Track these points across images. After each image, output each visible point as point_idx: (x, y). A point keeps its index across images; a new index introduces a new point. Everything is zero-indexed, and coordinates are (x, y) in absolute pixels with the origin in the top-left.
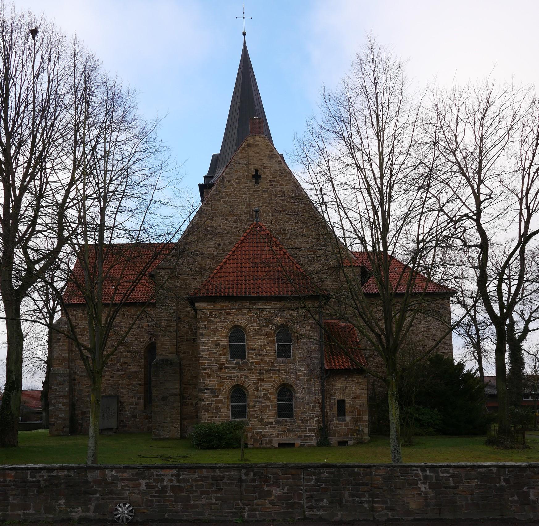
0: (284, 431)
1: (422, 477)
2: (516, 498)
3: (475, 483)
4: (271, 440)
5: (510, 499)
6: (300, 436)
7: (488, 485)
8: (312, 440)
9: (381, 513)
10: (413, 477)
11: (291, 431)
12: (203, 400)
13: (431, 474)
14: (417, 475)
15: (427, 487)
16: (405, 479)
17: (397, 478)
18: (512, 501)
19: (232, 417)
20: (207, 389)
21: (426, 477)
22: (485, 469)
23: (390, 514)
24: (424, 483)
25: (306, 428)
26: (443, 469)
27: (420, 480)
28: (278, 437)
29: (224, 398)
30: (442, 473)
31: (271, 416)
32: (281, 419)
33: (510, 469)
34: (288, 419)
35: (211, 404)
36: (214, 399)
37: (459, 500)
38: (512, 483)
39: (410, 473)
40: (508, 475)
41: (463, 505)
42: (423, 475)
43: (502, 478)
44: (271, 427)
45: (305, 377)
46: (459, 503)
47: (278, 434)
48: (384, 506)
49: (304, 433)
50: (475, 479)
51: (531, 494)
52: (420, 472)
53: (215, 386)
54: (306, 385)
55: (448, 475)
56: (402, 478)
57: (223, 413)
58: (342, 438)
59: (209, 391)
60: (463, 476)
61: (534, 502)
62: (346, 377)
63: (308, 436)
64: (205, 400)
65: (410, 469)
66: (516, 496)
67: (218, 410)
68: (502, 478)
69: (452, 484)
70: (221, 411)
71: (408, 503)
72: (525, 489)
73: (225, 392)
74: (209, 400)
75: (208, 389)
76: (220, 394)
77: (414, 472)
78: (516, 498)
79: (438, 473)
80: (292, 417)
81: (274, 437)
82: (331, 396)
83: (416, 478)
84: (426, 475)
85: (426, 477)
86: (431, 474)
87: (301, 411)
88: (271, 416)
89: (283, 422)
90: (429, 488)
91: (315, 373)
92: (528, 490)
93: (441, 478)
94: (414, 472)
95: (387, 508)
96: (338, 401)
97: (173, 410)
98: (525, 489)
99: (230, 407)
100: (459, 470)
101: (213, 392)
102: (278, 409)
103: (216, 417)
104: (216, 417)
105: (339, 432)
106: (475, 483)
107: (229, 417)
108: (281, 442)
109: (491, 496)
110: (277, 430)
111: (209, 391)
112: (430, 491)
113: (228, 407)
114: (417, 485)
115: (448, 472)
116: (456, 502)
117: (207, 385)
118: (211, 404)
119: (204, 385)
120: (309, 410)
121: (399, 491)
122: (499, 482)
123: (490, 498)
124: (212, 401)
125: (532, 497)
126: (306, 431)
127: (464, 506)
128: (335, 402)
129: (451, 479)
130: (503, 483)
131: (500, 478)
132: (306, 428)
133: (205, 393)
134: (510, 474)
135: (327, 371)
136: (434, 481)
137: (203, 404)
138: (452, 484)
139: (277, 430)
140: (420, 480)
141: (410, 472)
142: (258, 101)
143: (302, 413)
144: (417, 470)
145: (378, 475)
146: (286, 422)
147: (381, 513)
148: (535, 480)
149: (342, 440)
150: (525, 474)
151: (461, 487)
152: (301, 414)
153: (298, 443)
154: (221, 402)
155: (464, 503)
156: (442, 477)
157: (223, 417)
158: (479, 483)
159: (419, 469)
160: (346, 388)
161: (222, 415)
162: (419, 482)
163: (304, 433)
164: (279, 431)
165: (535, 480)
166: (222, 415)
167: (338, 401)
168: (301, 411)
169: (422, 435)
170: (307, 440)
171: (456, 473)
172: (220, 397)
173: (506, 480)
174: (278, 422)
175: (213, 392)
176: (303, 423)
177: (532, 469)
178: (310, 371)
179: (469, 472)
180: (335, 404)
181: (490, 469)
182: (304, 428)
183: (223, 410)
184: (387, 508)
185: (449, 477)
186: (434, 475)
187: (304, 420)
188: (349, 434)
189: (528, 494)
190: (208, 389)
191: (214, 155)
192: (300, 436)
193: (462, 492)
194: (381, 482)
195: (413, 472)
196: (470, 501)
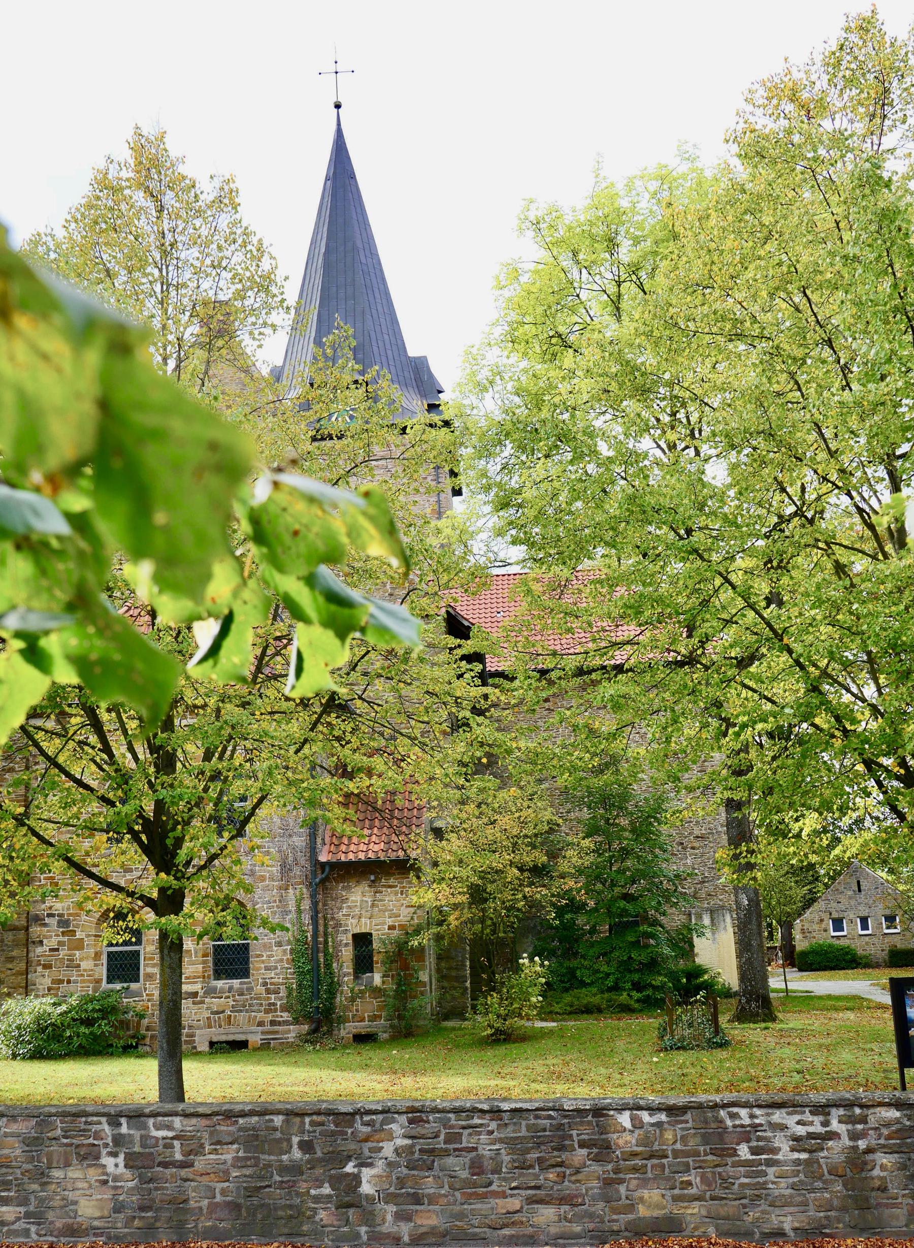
0: (223, 1012)
1: (109, 1140)
2: (327, 1190)
3: (229, 1154)
4: (193, 1035)
5: (313, 1192)
6: (261, 1024)
7: (262, 1157)
8: (289, 1031)
9: (12, 1227)
10: (91, 1141)
11: (241, 1011)
12: (41, 942)
13: (132, 1132)
14: (97, 1135)
15: (122, 1165)
16: (71, 1145)
17: (54, 1142)
18: (317, 1199)
19: (109, 981)
20: (49, 915)
21: (119, 1140)
22: (256, 1118)
23: (33, 1229)
24: (114, 1155)
25: (274, 1004)
26: (160, 1118)
27: (106, 1145)
28: (210, 1027)
29: (88, 936)
30: (157, 1129)
31: (195, 977)
32: (220, 984)
33: (315, 1117)
34: (236, 983)
35: (57, 950)
36: (66, 939)
37: (194, 1194)
38: (319, 1154)
39: (84, 1130)
40: (309, 1132)
41: (201, 1208)
42: (113, 1135)
43: (295, 1140)
44: (194, 1003)
45: (273, 880)
46: (192, 1203)
47: (208, 1018)
48: (22, 1209)
49: (270, 1017)
50: (231, 1143)
51: (364, 1180)
52: (106, 1127)
53: (68, 909)
54: (275, 901)
55: (170, 1134)
56: (65, 1141)
57: (85, 970)
58: (361, 1027)
59: (53, 922)
60: (206, 1135)
61: (370, 1199)
62: (372, 878)
63: (279, 1024)
64: (45, 941)
65: (83, 1119)
66: (326, 1185)
67: (72, 965)
68: (295, 1140)
69: (178, 1156)
70: (79, 966)
71: (75, 1203)
72: (350, 1168)
73: (91, 922)
74: (53, 942)
75: (52, 915)
76: (77, 926)
77: (94, 1128)
78: (327, 1190)
79: (145, 1127)
80: (247, 976)
81: (199, 1028)
82: (338, 925)
83: (96, 1142)
84: (120, 1134)
85: (119, 1140)
86: (132, 1132)
87: (263, 962)
88: (195, 977)
89: (222, 991)
90: (126, 1166)
91: (297, 871)
92: (356, 1170)
93: (153, 1141)
94: (94, 1128)
95: (28, 1215)
96: (355, 936)
97: (10, 966)
98: (350, 1168)
99: (104, 959)
100: (194, 1121)
101: (64, 923)
102: (214, 960)
103: (69, 982)
104: (69, 982)
105: (357, 1011)
106: (229, 1154)
107: (98, 981)
108: (215, 1039)
109: (269, 1186)
110: (207, 1009)
111: (53, 922)
112: (128, 1174)
113: (97, 956)
114: (98, 1157)
115: (169, 1127)
116: (186, 1201)
117: (51, 908)
118: (57, 950)
119: (43, 906)
120: (281, 960)
121: (57, 1174)
122: (289, 1151)
123: (267, 1190)
124: (59, 943)
125: (366, 1188)
126: (276, 1011)
127: (205, 1211)
128: (347, 939)
129: (177, 1143)
130: (297, 1154)
131: (289, 1141)
132: (274, 1004)
133: (45, 925)
134: (315, 1131)
135: (323, 865)
136: (137, 1149)
137: (39, 950)
138: (178, 1156)
139: (207, 1009)
140: (106, 1145)
141: (83, 1126)
142: (366, 246)
143: (267, 969)
144: (100, 1123)
145: (12, 1135)
146: (230, 989)
147: (12, 1227)
148: (375, 1144)
149: (363, 1032)
150: (350, 1131)
151: (200, 1163)
152: (263, 971)
153: (255, 1039)
154: (79, 945)
155: (205, 1202)
156: (157, 1139)
157: (83, 981)
158: (241, 1154)
159: (104, 1120)
160: (373, 905)
161: (82, 975)
162: (104, 1152)
163: (270, 1017)
164: (212, 1013)
165: (375, 1144)
166: (82, 975)
167: (355, 936)
168: (263, 962)
169: (600, 1011)
170: (277, 1032)
171: (188, 1129)
172: (79, 935)
173: (306, 1147)
174: (210, 992)
175: (64, 923)
176: (268, 991)
177: (367, 1118)
178: (285, 869)
179: (218, 1127)
180: (347, 945)
181: (267, 1117)
182: (270, 1004)
183: (85, 965)
184: (28, 1215)
185: (172, 1138)
186: (136, 1134)
187: (272, 984)
188: (380, 1017)
189: (356, 1179)
190: (52, 915)
191: (425, 357)
192: (261, 1024)
193: (202, 1175)
194: (18, 1152)
195: (90, 1127)
196: (219, 1198)
